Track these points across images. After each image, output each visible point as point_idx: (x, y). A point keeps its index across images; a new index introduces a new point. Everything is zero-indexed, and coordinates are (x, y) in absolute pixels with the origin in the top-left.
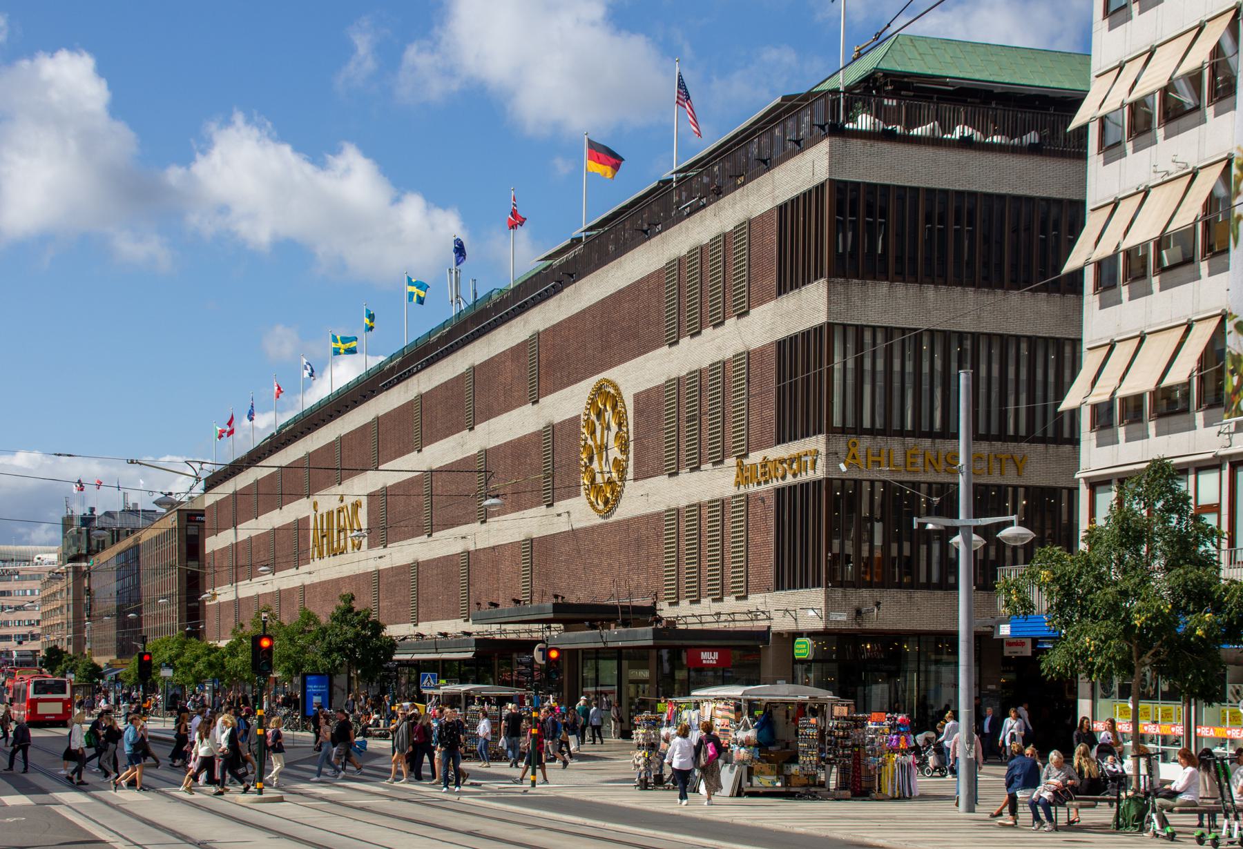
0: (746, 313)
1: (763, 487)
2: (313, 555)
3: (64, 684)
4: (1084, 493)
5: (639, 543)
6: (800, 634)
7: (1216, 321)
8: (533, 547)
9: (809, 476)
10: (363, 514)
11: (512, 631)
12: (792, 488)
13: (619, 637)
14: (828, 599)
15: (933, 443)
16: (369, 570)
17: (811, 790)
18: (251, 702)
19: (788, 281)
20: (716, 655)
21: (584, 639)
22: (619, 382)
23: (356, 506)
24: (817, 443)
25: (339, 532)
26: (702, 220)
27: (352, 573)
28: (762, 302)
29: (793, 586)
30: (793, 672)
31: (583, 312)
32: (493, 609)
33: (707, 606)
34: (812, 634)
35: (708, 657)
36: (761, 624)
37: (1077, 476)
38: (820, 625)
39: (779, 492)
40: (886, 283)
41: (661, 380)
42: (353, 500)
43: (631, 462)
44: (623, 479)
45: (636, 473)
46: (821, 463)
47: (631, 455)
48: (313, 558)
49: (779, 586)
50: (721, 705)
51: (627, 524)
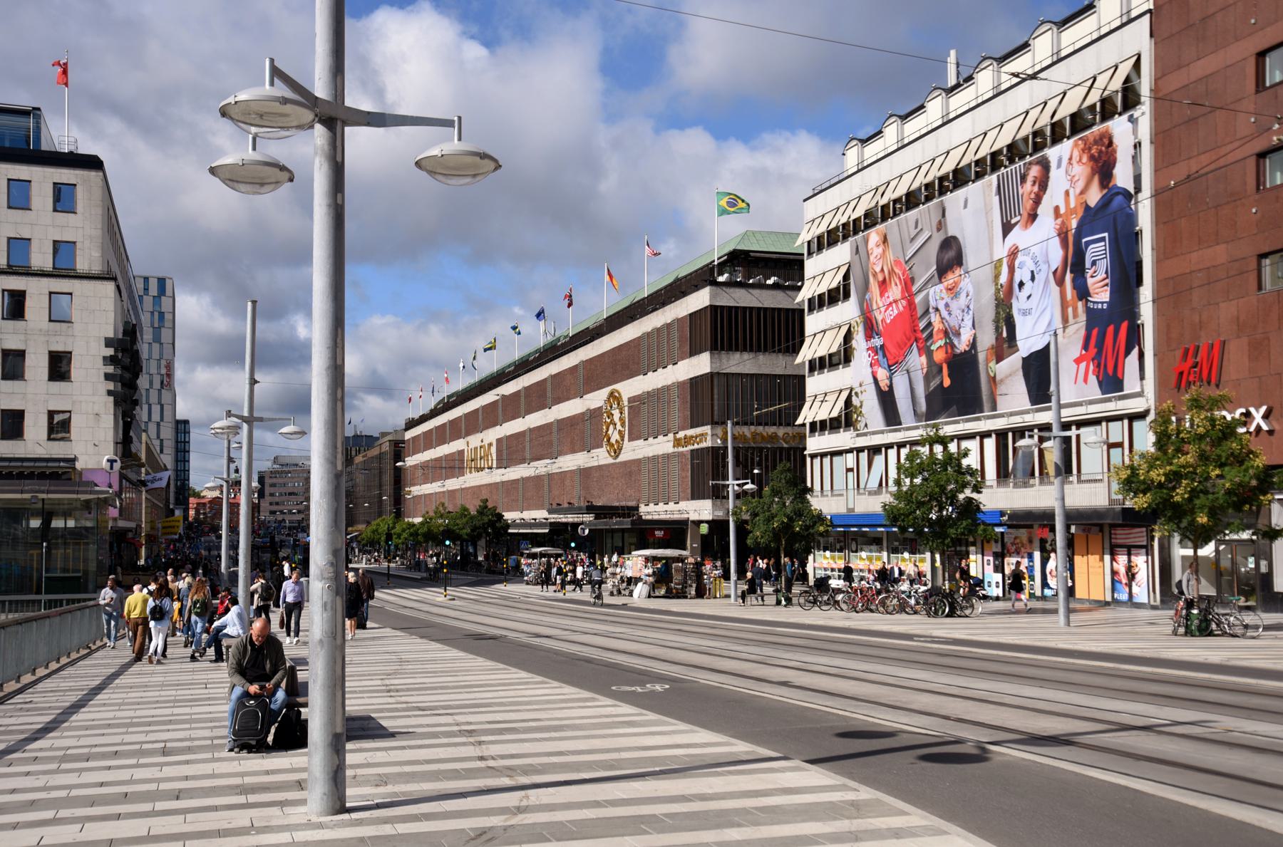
0: (676, 363)
1: (685, 449)
4: (808, 460)
5: (630, 474)
6: (702, 522)
7: (849, 391)
8: (585, 473)
9: (704, 445)
10: (494, 449)
11: (570, 518)
12: (697, 450)
13: (616, 523)
14: (713, 504)
15: (764, 429)
17: (681, 595)
19: (694, 352)
20: (663, 532)
21: (603, 524)
22: (621, 391)
23: (490, 445)
24: (707, 429)
25: (481, 459)
26: (657, 315)
28: (683, 359)
29: (699, 498)
31: (602, 355)
32: (559, 507)
33: (661, 507)
34: (707, 522)
35: (659, 534)
36: (686, 516)
37: (805, 453)
38: (710, 518)
39: (692, 451)
40: (739, 353)
41: (640, 392)
42: (489, 442)
43: (627, 432)
44: (623, 440)
45: (629, 438)
46: (709, 438)
47: (627, 428)
49: (693, 498)
50: (640, 558)
51: (625, 463)
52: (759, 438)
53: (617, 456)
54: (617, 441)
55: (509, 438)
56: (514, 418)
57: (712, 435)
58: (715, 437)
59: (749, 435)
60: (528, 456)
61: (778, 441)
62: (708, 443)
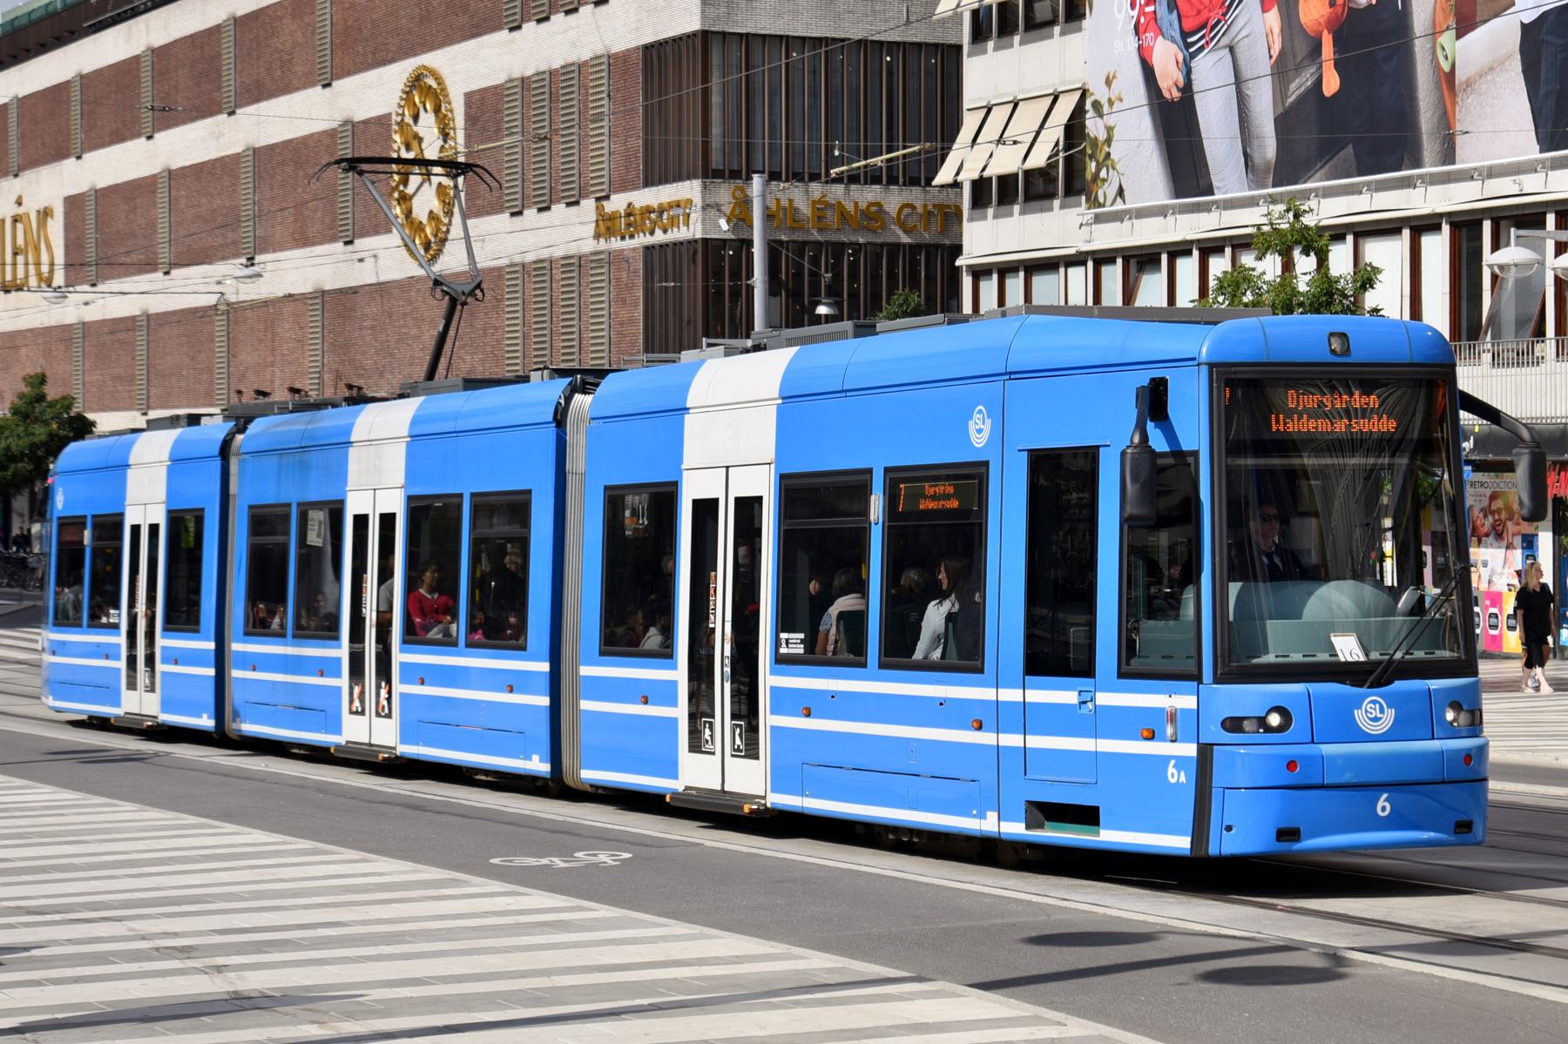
1: (628, 244)
10: (56, 230)
23: (46, 214)
24: (690, 190)
52: (832, 218)
53: (434, 259)
54: (432, 216)
55: (103, 196)
56: (118, 137)
57: (705, 208)
58: (713, 212)
59: (805, 209)
60: (164, 253)
61: (884, 227)
62: (693, 230)
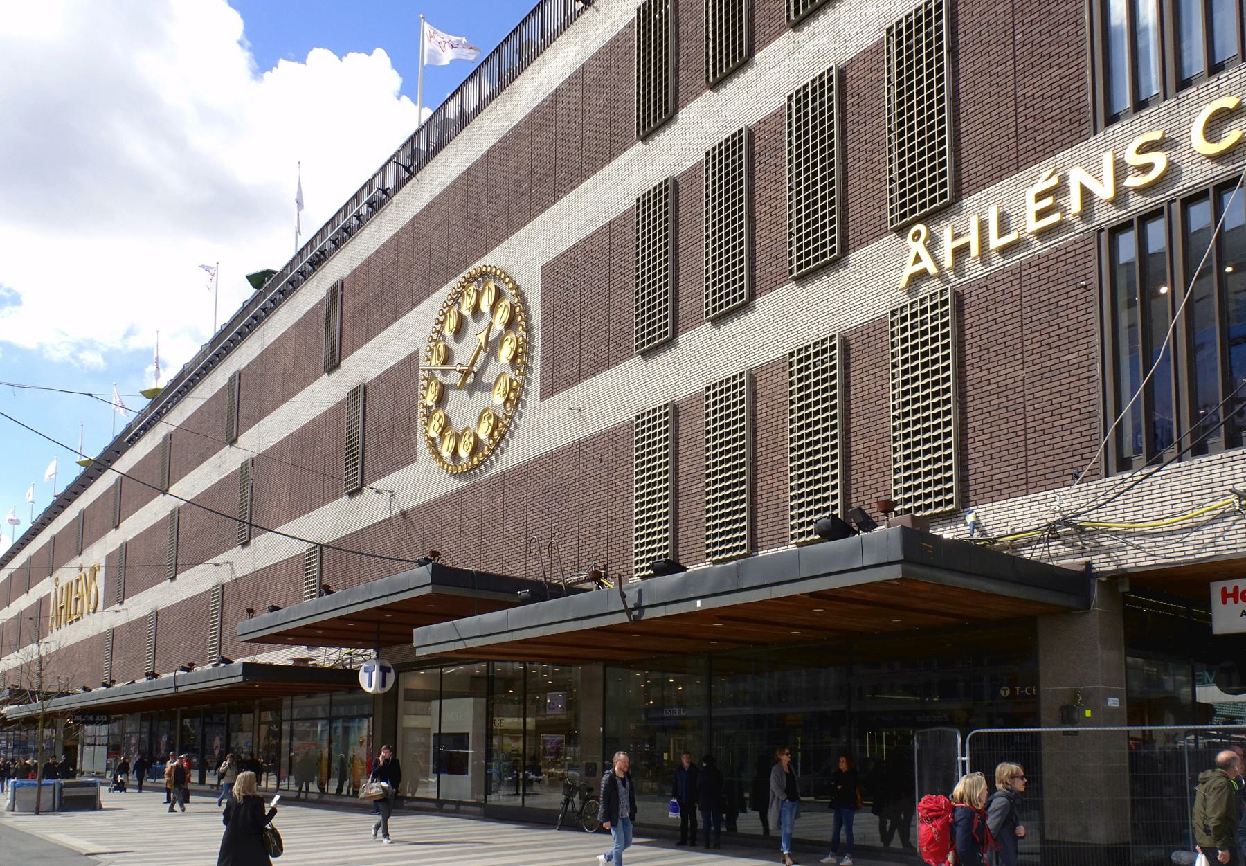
2: (52, 627)
3: (309, 732)
16: (103, 631)
18: (217, 752)
27: (86, 637)
30: (963, 572)
48: (52, 631)
